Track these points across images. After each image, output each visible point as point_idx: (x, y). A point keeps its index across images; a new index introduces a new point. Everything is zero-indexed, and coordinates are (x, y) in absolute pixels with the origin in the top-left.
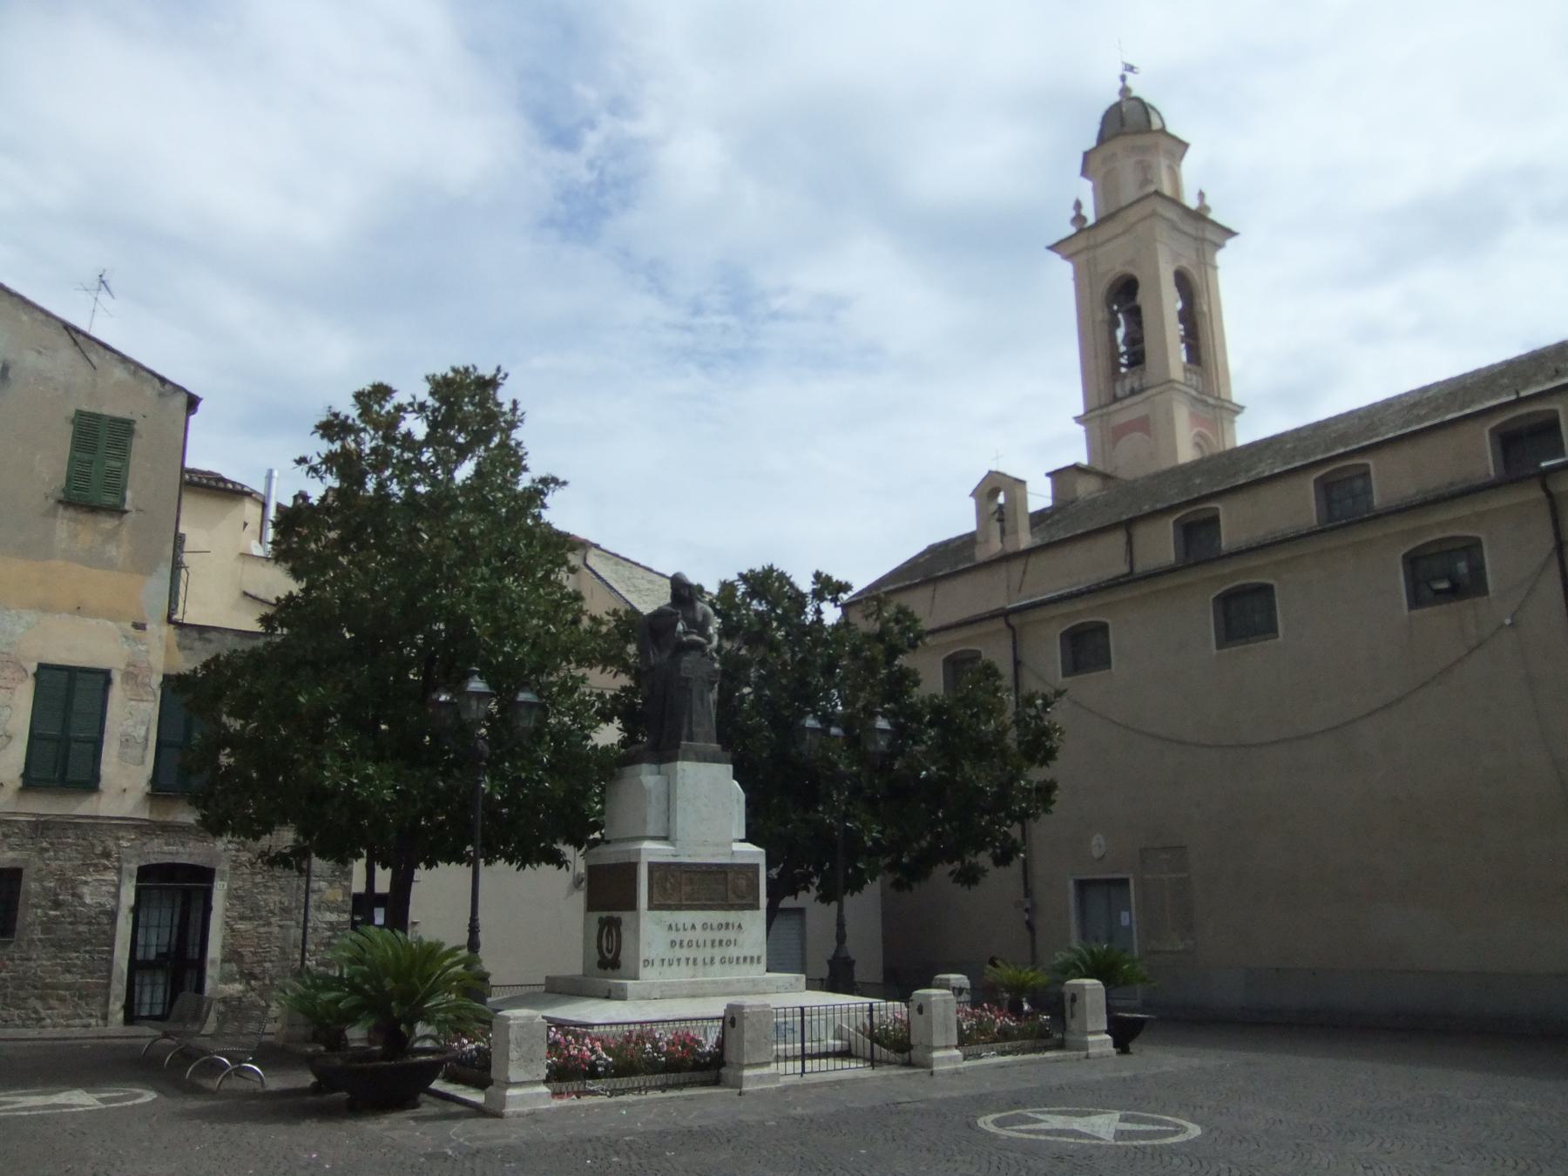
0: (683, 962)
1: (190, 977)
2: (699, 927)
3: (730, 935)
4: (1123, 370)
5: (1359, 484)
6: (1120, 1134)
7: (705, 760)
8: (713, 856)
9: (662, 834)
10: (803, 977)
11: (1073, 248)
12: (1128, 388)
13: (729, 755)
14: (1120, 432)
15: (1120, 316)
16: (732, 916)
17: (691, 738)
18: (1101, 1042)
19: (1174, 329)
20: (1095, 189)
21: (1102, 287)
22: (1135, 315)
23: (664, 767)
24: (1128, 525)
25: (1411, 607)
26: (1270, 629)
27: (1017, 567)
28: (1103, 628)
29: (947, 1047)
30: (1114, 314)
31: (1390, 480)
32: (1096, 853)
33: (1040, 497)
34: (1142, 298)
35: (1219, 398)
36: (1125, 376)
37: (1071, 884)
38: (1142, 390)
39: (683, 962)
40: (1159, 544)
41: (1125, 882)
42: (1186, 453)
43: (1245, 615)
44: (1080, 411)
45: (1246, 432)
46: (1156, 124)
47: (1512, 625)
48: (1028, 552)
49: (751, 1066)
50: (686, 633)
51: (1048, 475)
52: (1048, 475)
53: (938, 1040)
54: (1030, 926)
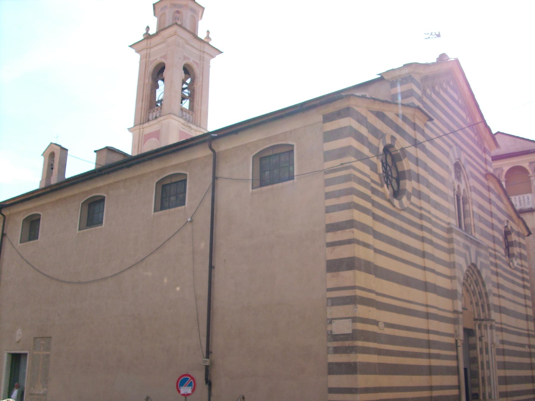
12: (154, 116)
21: (151, 68)
32: (18, 338)
44: (132, 125)
47: (191, 221)
51: (95, 151)
52: (95, 151)
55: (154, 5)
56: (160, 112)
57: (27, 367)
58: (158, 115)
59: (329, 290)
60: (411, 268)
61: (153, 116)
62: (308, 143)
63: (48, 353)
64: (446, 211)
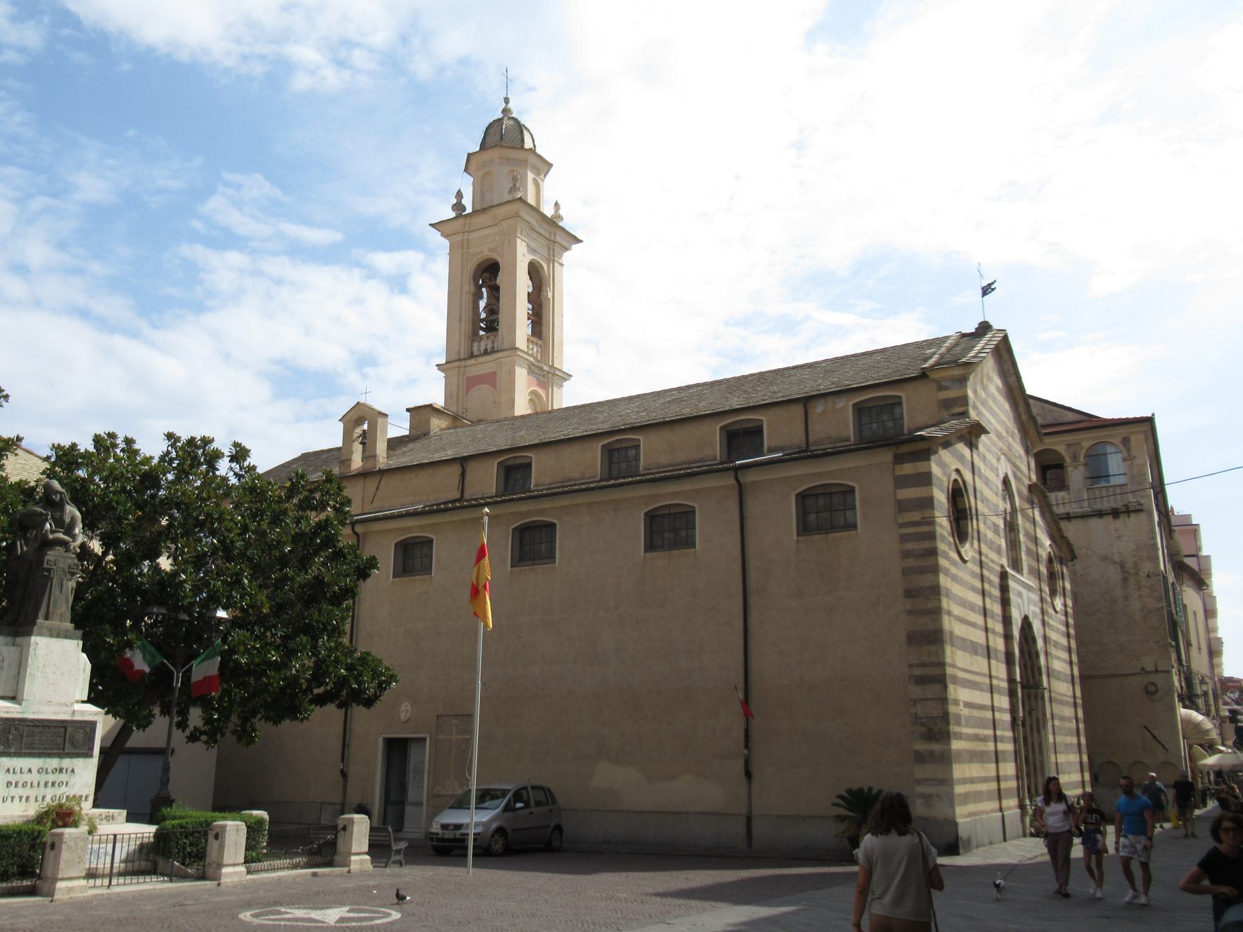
0: (17, 799)
1: (318, 859)
2: (34, 771)
3: (63, 777)
4: (482, 333)
5: (632, 453)
6: (342, 920)
7: (58, 636)
8: (55, 713)
9: (12, 695)
10: (124, 812)
11: (449, 228)
13: (80, 633)
14: (472, 382)
15: (484, 290)
16: (67, 763)
17: (47, 618)
18: (360, 859)
19: (523, 308)
20: (474, 184)
21: (471, 265)
22: (495, 290)
23: (18, 640)
24: (463, 461)
25: (646, 551)
26: (551, 556)
27: (371, 483)
28: (430, 542)
29: (234, 865)
30: (479, 288)
31: (653, 452)
32: (403, 717)
33: (399, 427)
34: (501, 280)
35: (552, 366)
36: (481, 338)
37: (381, 741)
38: (493, 351)
39: (17, 799)
40: (486, 480)
41: (424, 739)
42: (522, 407)
43: (533, 544)
45: (569, 396)
46: (528, 144)
48: (382, 472)
49: (63, 879)
50: (52, 532)
51: (408, 410)
52: (408, 410)
53: (227, 859)
54: (344, 774)
57: (422, 759)
58: (489, 348)
59: (910, 666)
60: (422, 478)
61: (479, 346)
62: (780, 432)
63: (468, 737)
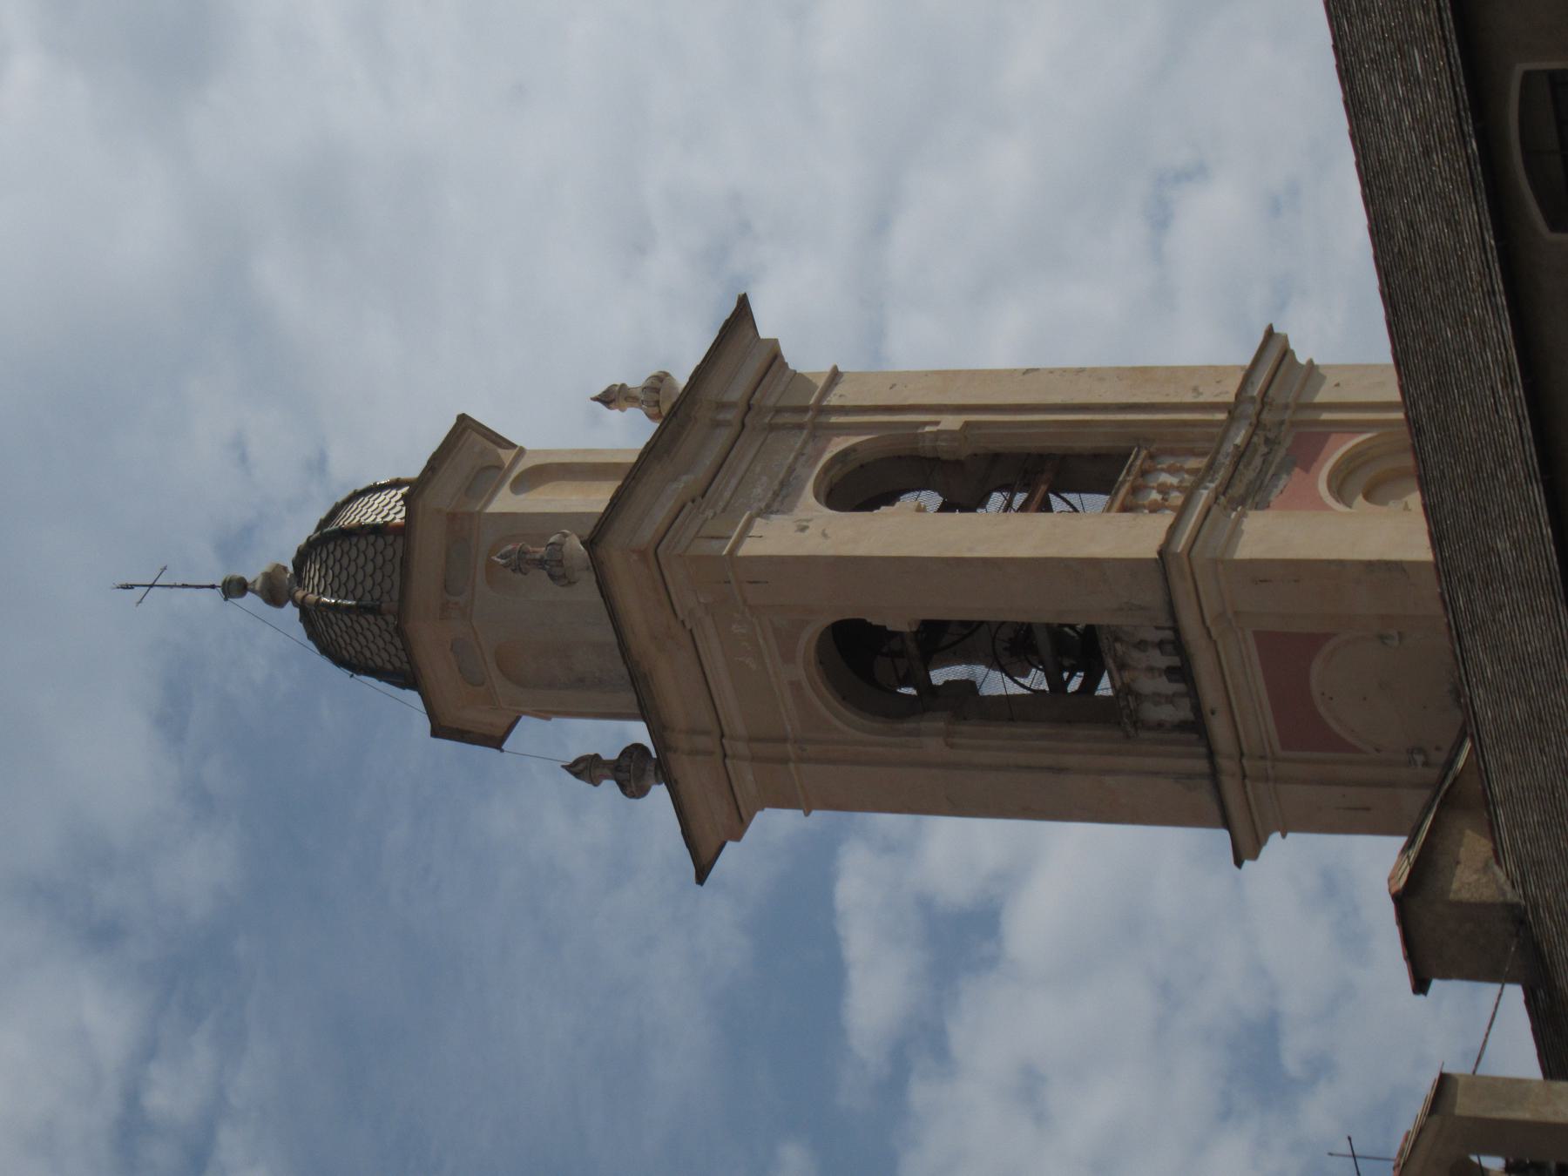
12: (1165, 686)
52: (1420, 986)
55: (437, 732)
56: (1142, 645)
61: (1158, 699)
64: (1170, 699)
